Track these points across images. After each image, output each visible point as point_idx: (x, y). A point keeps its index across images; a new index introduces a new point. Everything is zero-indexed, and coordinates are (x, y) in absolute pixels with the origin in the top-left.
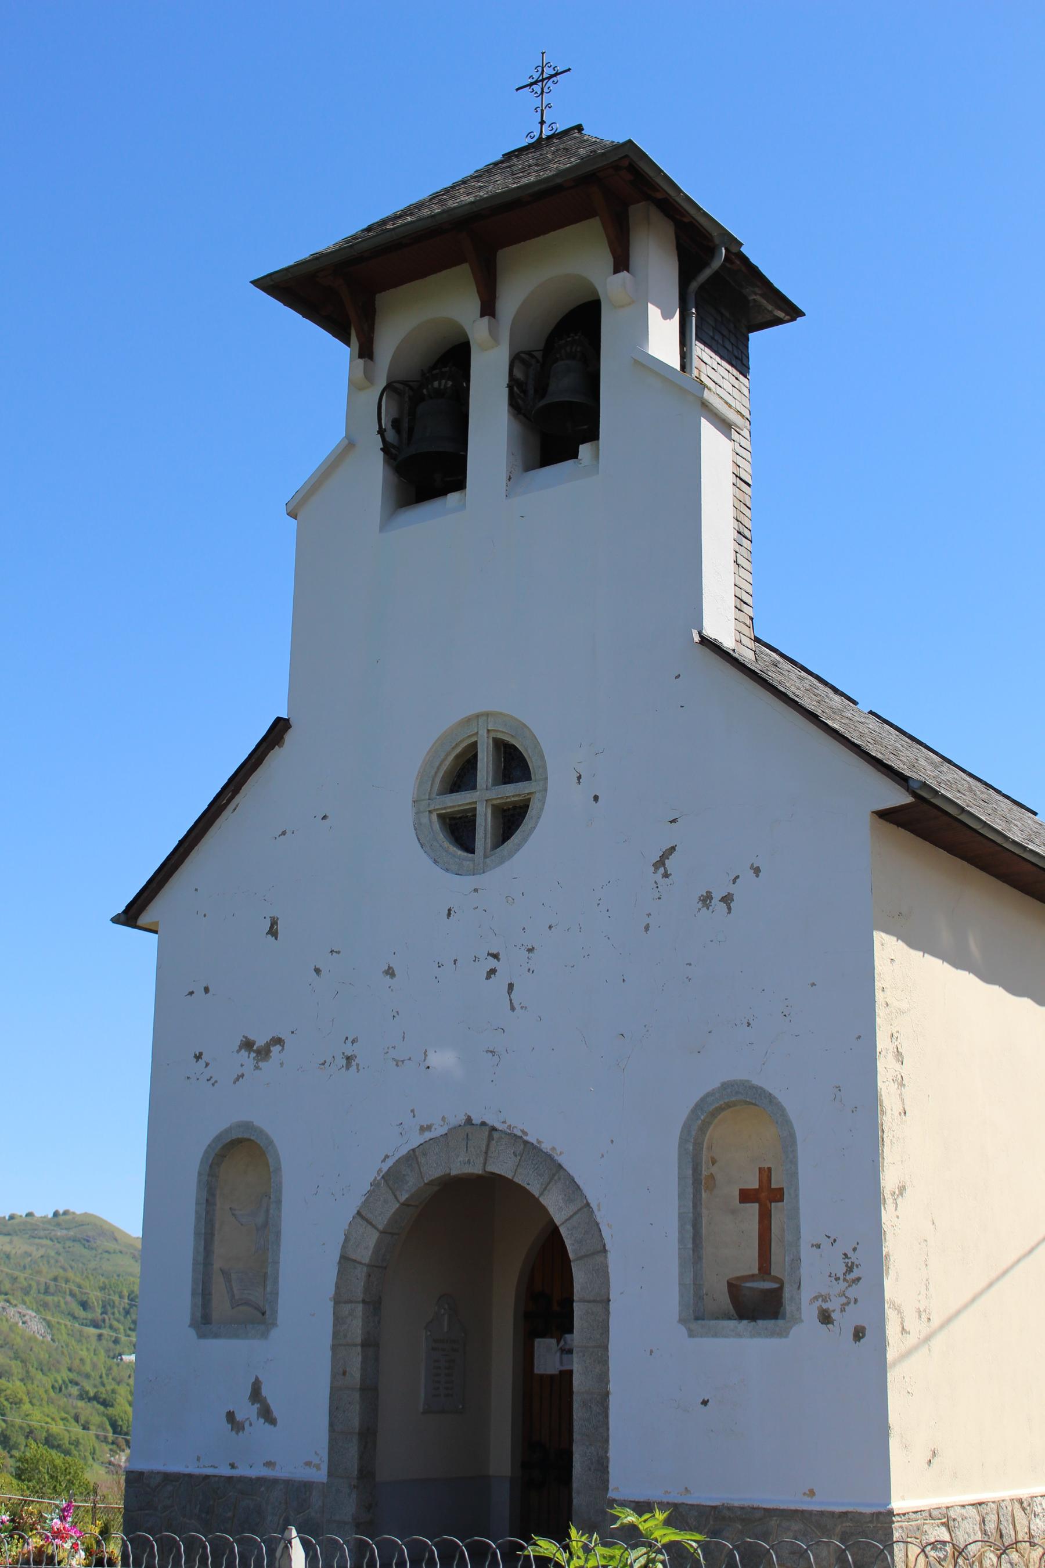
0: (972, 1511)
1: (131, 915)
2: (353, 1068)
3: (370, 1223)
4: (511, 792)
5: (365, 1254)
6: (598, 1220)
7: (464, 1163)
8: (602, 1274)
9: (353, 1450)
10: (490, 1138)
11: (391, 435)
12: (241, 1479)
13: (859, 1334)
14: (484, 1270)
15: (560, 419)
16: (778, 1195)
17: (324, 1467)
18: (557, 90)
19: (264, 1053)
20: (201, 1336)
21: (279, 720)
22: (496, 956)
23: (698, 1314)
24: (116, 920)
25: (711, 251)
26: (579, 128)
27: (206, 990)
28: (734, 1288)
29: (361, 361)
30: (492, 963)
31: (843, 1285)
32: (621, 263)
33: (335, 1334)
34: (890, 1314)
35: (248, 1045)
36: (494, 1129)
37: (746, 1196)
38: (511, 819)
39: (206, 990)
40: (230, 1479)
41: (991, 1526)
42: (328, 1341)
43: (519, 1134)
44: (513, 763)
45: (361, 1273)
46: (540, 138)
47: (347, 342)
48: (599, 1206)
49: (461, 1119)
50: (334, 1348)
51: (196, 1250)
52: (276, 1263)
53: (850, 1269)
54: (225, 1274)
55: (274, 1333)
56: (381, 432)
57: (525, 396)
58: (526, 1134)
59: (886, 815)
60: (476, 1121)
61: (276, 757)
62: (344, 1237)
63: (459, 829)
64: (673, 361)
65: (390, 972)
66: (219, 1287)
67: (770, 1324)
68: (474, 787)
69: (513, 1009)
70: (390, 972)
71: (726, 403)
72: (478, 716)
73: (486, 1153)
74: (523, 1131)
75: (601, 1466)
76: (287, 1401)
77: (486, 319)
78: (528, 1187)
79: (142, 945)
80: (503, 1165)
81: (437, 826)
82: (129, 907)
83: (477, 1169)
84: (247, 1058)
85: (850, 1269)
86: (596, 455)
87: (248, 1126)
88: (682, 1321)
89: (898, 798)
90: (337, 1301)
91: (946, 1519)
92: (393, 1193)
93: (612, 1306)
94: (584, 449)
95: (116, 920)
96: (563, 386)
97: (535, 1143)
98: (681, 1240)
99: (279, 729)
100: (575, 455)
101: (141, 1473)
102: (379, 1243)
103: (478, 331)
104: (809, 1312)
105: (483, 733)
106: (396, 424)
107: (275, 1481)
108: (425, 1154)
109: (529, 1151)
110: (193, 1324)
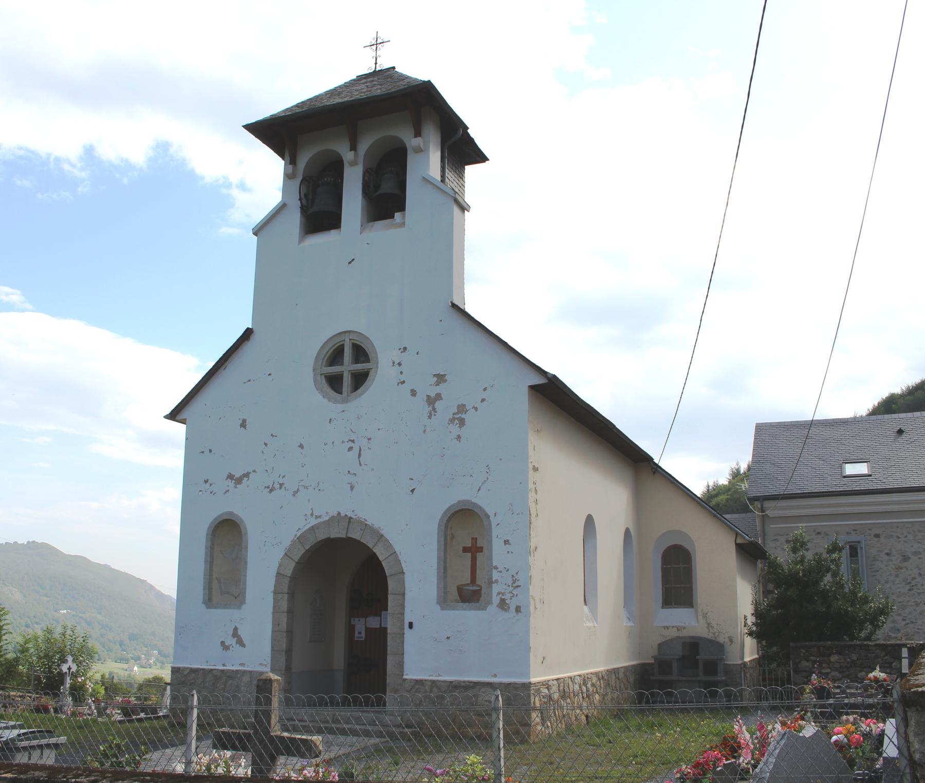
0: (555, 682)
1: (174, 415)
2: (283, 489)
4: (360, 367)
5: (289, 572)
7: (337, 533)
9: (283, 659)
11: (304, 201)
12: (228, 671)
13: (518, 609)
14: (343, 580)
15: (386, 202)
16: (480, 550)
17: (269, 666)
18: (382, 50)
19: (239, 481)
20: (208, 607)
21: (248, 329)
22: (353, 441)
23: (444, 601)
24: (166, 417)
25: (457, 131)
26: (394, 68)
27: (210, 451)
28: (460, 589)
29: (291, 166)
30: (351, 444)
31: (511, 589)
32: (418, 134)
33: (274, 607)
34: (532, 601)
35: (230, 477)
36: (351, 518)
37: (465, 550)
38: (360, 379)
39: (210, 451)
40: (223, 671)
41: (561, 688)
42: (271, 610)
44: (361, 353)
45: (287, 580)
46: (375, 71)
47: (283, 159)
50: (274, 613)
51: (205, 568)
52: (245, 576)
53: (514, 582)
54: (219, 580)
55: (244, 607)
56: (300, 199)
57: (369, 190)
59: (533, 388)
61: (248, 347)
63: (334, 382)
64: (438, 177)
65: (301, 446)
66: (215, 585)
67: (474, 604)
68: (342, 364)
69: (360, 465)
70: (301, 446)
72: (345, 332)
75: (400, 665)
76: (252, 638)
77: (353, 152)
79: (179, 430)
80: (355, 535)
81: (324, 381)
82: (172, 411)
84: (231, 484)
85: (514, 582)
86: (404, 217)
87: (231, 513)
88: (438, 603)
89: (540, 380)
90: (275, 593)
91: (547, 685)
93: (406, 597)
94: (397, 215)
95: (166, 417)
96: (387, 187)
98: (438, 568)
99: (248, 334)
100: (393, 217)
101: (179, 668)
102: (295, 567)
103: (348, 156)
104: (496, 600)
105: (347, 340)
106: (306, 195)
107: (244, 672)
109: (365, 527)
110: (204, 602)
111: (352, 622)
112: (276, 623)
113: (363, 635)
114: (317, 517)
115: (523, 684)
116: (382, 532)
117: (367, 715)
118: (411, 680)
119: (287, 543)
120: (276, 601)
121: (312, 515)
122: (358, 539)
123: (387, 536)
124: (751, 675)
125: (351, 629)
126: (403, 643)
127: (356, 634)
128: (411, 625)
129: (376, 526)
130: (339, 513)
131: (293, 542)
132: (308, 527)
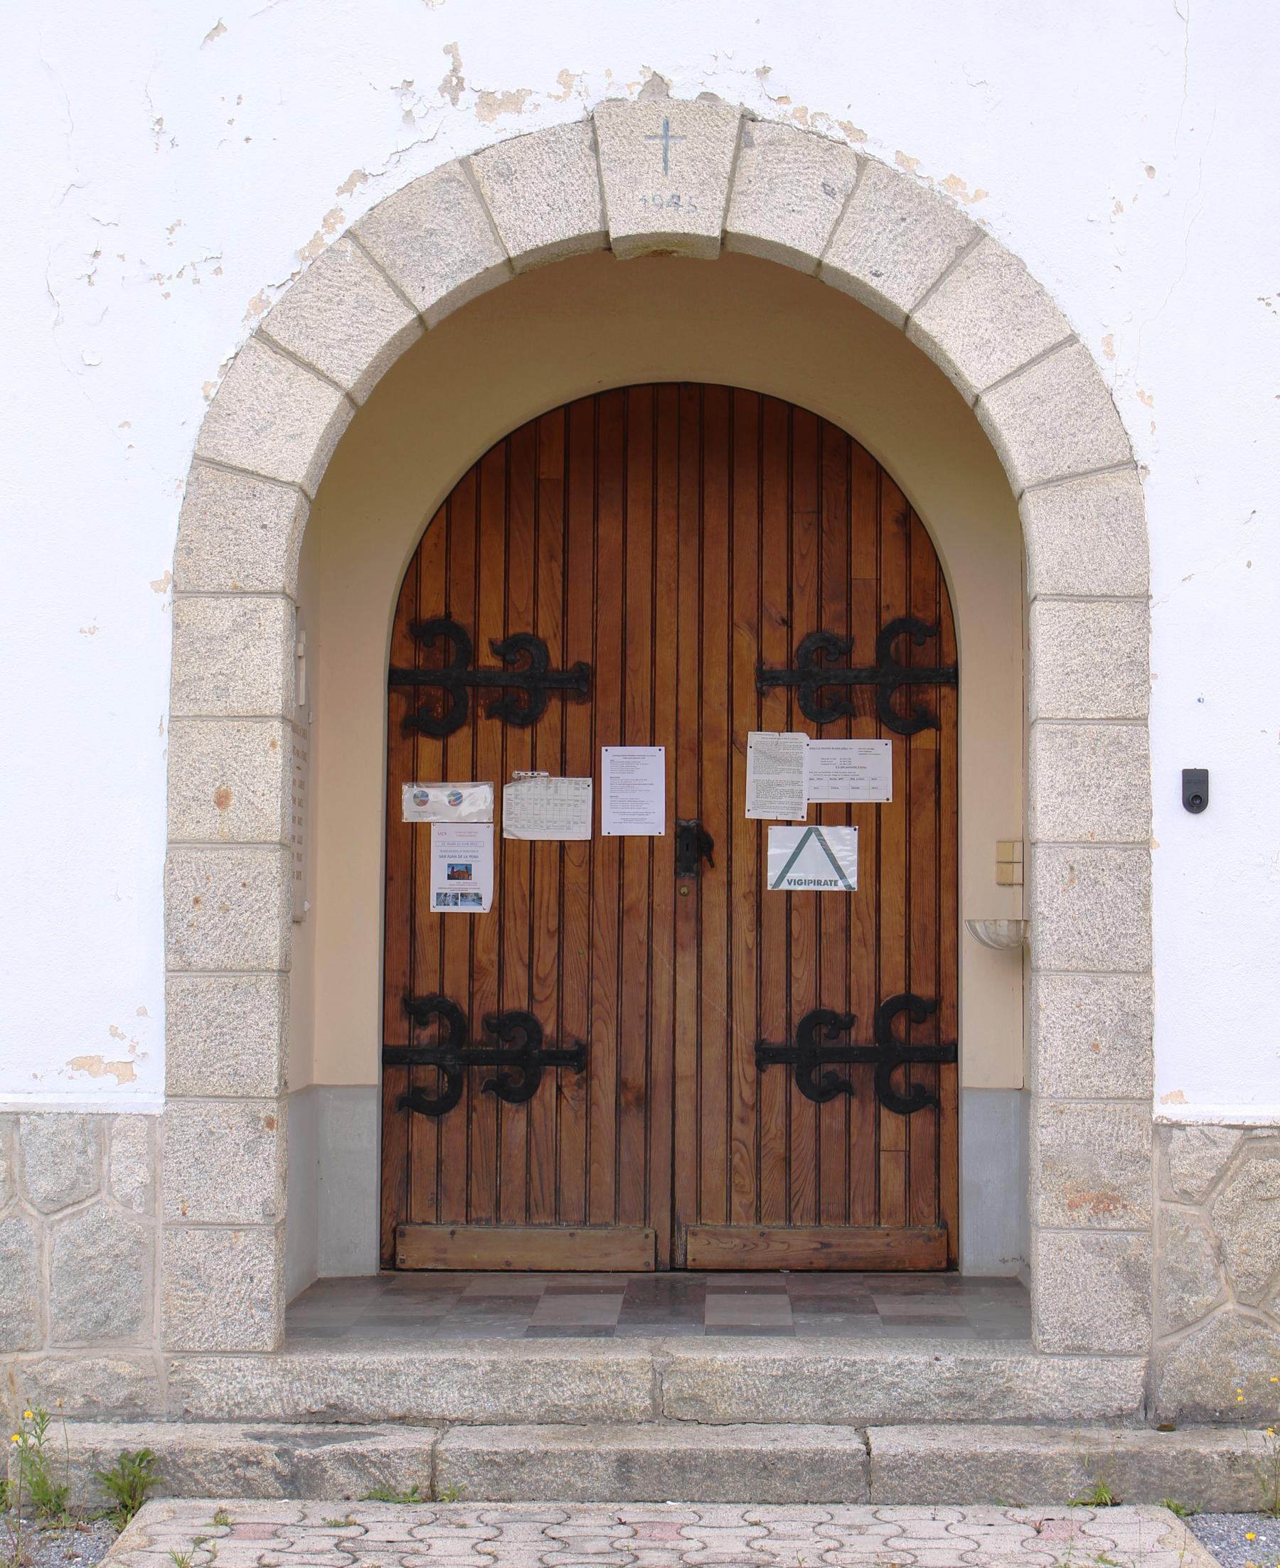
3: (310, 367)
6: (1108, 378)
8: (1022, 293)
10: (743, 140)
36: (748, 117)
42: (159, 702)
43: (839, 134)
48: (1108, 341)
49: (629, 85)
58: (861, 136)
60: (684, 89)
62: (204, 407)
71: (508, 1270)
73: (731, 181)
74: (847, 128)
75: (1131, 1037)
78: (874, 283)
80: (786, 219)
83: (700, 221)
92: (392, 283)
97: (890, 161)
108: (506, 175)
111: (410, 813)
112: (198, 796)
113: (483, 881)
114: (488, 103)
115: (328, 1336)
116: (976, 212)
117: (902, 1359)
118: (1207, 1132)
119: (271, 261)
120: (188, 641)
121: (453, 86)
122: (811, 247)
123: (1008, 232)
124: (1175, 1348)
125: (405, 849)
126: (1144, 898)
127: (439, 881)
128: (1195, 793)
129: (932, 170)
130: (657, 85)
131: (317, 266)
132: (421, 164)
